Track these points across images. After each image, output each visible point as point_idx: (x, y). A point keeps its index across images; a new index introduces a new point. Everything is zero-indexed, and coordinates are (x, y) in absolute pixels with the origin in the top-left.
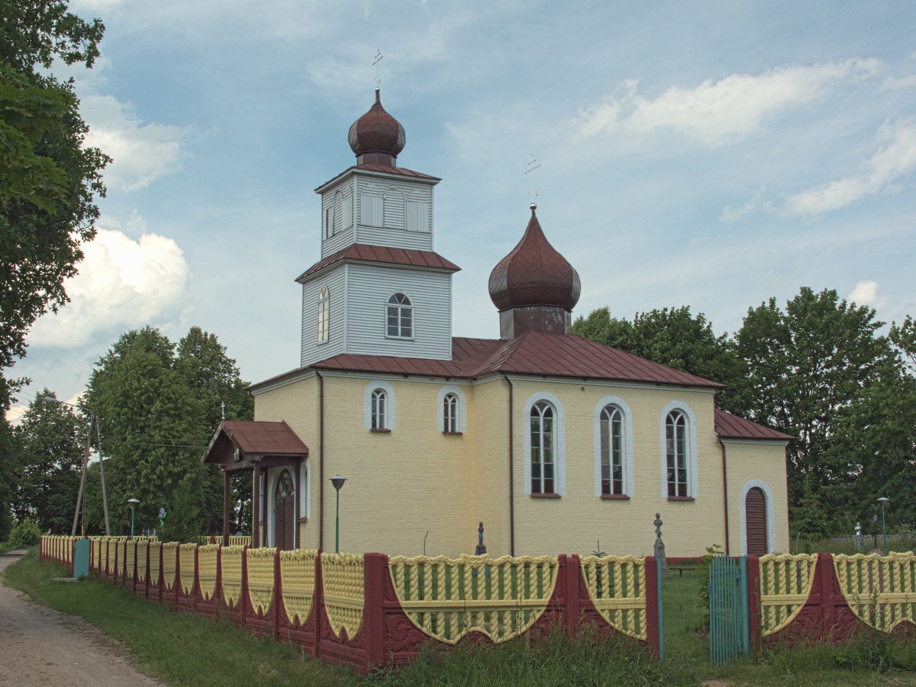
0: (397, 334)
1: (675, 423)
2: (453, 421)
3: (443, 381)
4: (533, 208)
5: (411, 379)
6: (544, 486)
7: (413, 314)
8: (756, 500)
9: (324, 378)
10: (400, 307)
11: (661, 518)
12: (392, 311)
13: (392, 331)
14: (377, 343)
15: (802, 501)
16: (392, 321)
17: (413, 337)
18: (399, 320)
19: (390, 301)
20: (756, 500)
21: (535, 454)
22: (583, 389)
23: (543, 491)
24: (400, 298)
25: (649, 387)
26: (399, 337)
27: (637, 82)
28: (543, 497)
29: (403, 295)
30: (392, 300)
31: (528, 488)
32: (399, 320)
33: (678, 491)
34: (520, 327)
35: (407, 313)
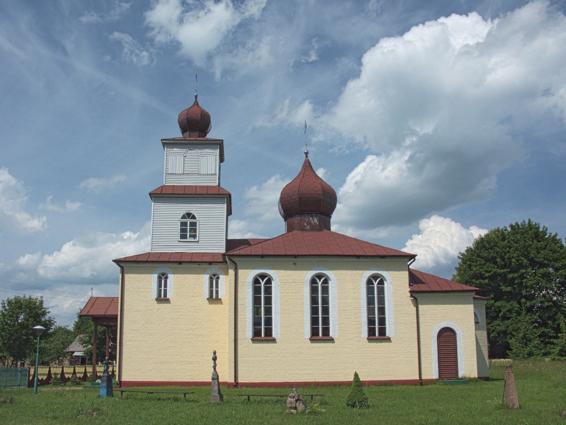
0: (186, 238)
1: (320, 283)
2: (165, 291)
3: (207, 266)
4: (306, 154)
5: (184, 265)
6: (263, 331)
7: (198, 225)
8: (447, 337)
9: (125, 268)
10: (189, 221)
11: (217, 355)
12: (183, 224)
13: (183, 236)
14: (174, 245)
15: (560, 335)
16: (183, 230)
17: (197, 239)
18: (188, 228)
19: (182, 218)
20: (447, 337)
21: (256, 311)
22: (295, 264)
23: (263, 335)
24: (189, 215)
25: (350, 259)
26: (188, 240)
27: (130, 4)
28: (262, 341)
29: (191, 214)
30: (184, 217)
31: (249, 333)
32: (188, 228)
33: (377, 331)
34: (290, 228)
35: (193, 224)
